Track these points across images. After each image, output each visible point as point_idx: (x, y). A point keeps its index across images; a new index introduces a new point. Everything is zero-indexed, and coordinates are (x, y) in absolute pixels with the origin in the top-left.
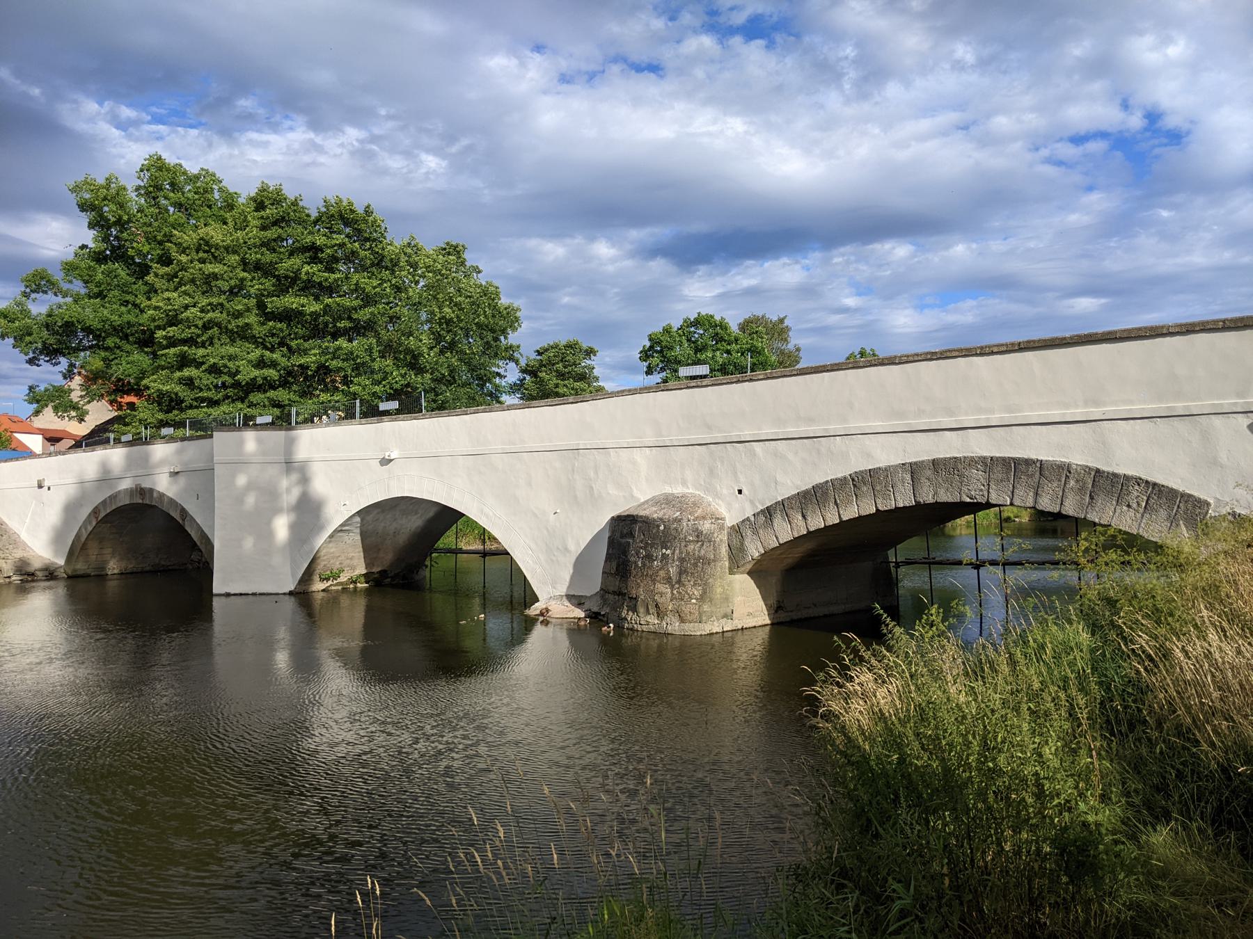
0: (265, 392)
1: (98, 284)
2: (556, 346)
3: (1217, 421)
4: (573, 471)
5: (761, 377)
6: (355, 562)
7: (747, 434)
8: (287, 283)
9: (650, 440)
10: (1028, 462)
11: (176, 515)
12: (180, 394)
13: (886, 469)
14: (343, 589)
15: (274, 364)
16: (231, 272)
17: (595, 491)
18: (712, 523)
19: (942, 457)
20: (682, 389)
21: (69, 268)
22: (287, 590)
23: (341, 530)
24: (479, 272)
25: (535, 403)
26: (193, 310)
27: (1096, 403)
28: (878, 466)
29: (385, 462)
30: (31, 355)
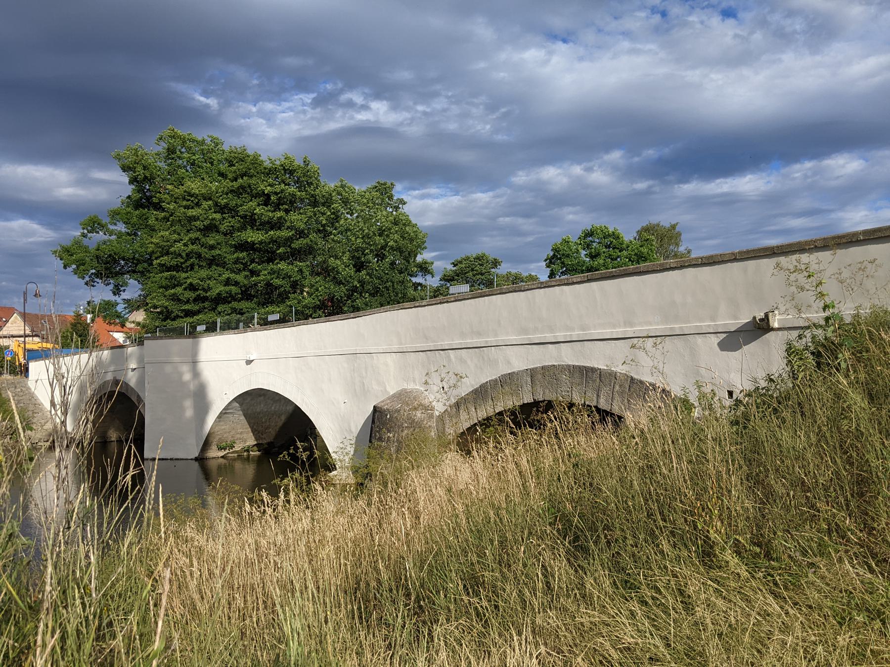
0: (229, 302)
1: (133, 225)
2: (467, 258)
3: (699, 340)
4: (354, 370)
5: (452, 300)
6: (245, 436)
7: (446, 344)
8: (250, 221)
9: (395, 347)
10: (593, 370)
11: (134, 399)
12: (169, 307)
13: (518, 373)
14: (238, 456)
15: (236, 284)
16: (205, 214)
17: (366, 386)
18: (422, 413)
19: (547, 364)
20: (411, 308)
21: (115, 215)
22: (193, 457)
23: (226, 413)
24: (405, 203)
25: (332, 318)
26: (179, 245)
27: (631, 324)
28: (513, 371)
29: (249, 362)
30: (87, 279)
